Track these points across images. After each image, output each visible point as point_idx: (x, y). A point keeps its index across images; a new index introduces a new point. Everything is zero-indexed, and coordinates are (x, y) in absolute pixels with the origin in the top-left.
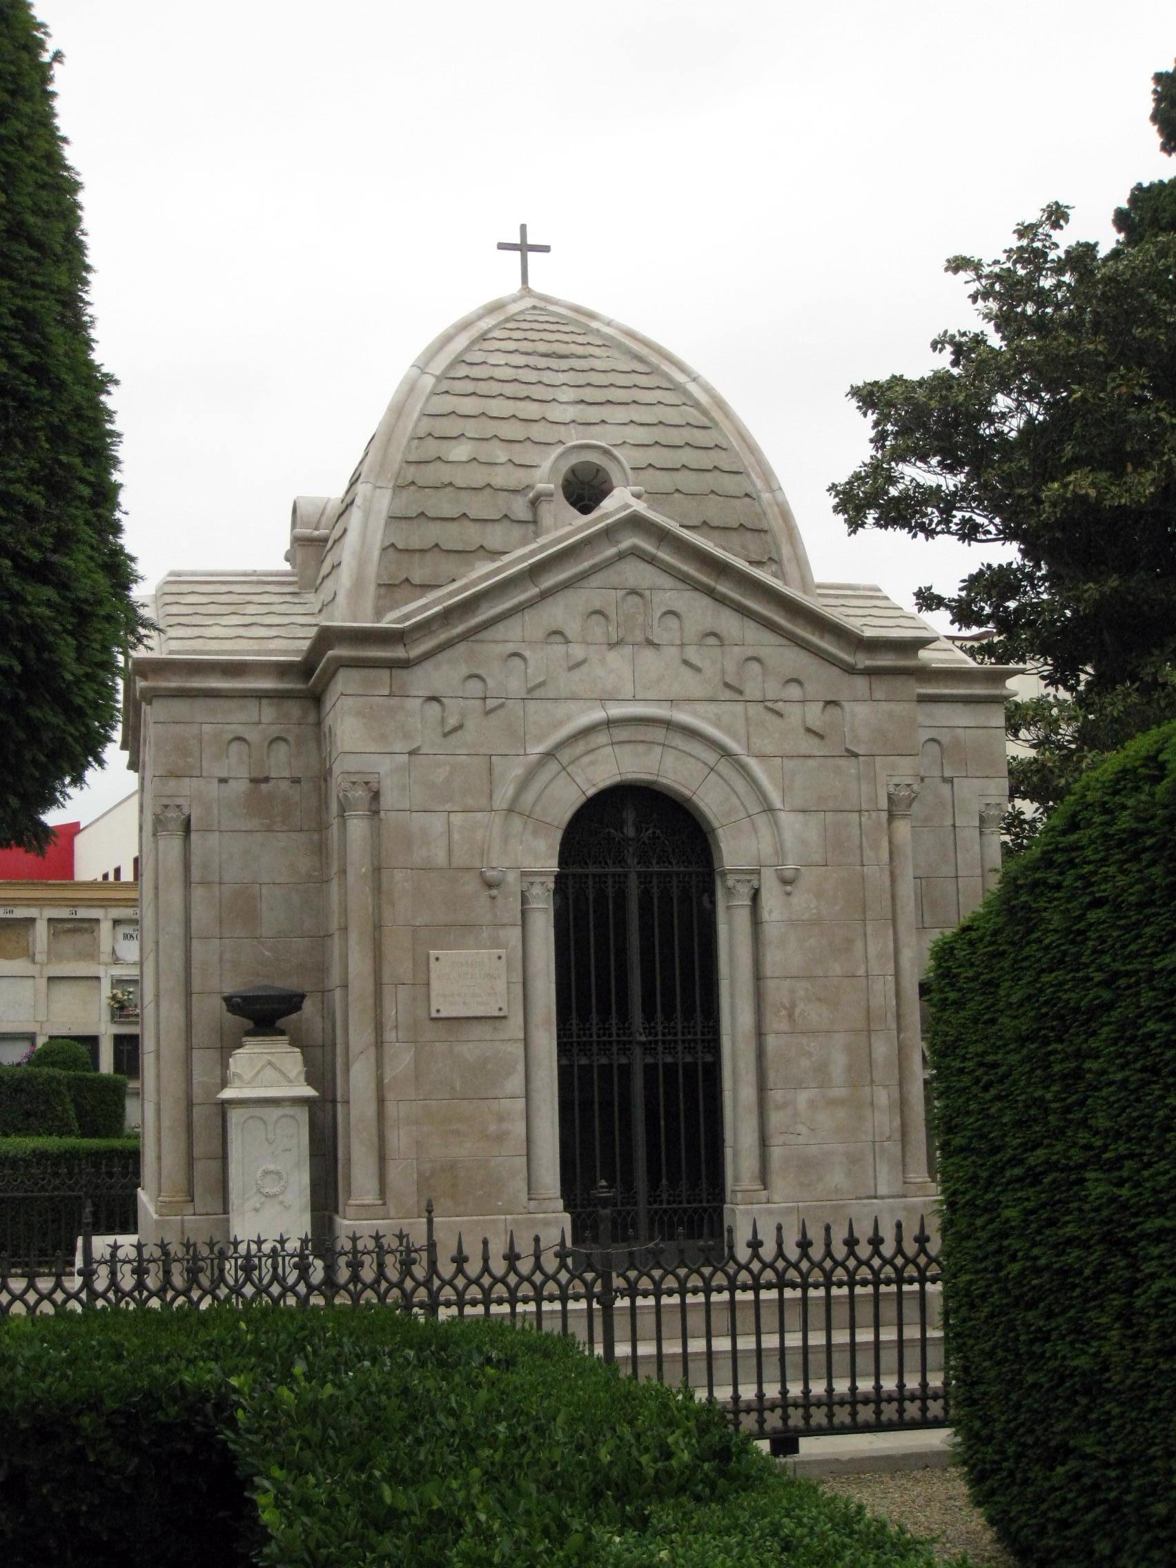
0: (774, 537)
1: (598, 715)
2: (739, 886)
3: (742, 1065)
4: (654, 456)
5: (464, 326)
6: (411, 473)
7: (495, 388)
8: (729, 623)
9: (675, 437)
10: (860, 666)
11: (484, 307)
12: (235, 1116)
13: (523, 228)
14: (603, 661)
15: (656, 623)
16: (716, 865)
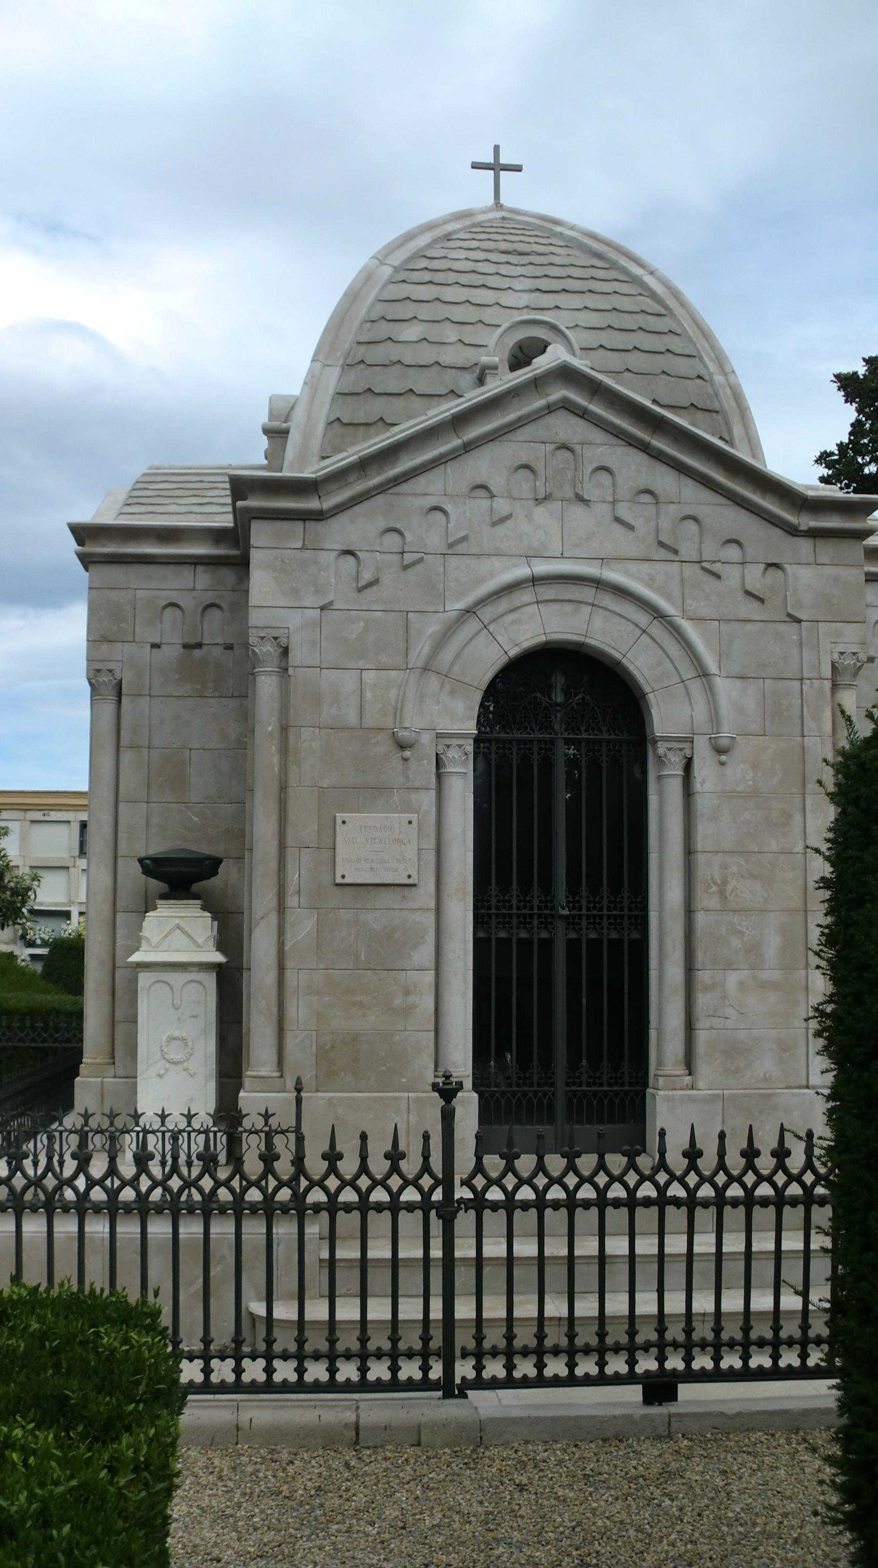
0: (726, 418)
1: (522, 571)
2: (670, 755)
3: (669, 944)
4: (605, 338)
5: (431, 226)
6: (361, 353)
7: (452, 277)
8: (665, 480)
9: (629, 322)
10: (803, 527)
11: (452, 214)
12: (144, 979)
13: (497, 149)
14: (529, 518)
15: (586, 478)
16: (648, 732)
